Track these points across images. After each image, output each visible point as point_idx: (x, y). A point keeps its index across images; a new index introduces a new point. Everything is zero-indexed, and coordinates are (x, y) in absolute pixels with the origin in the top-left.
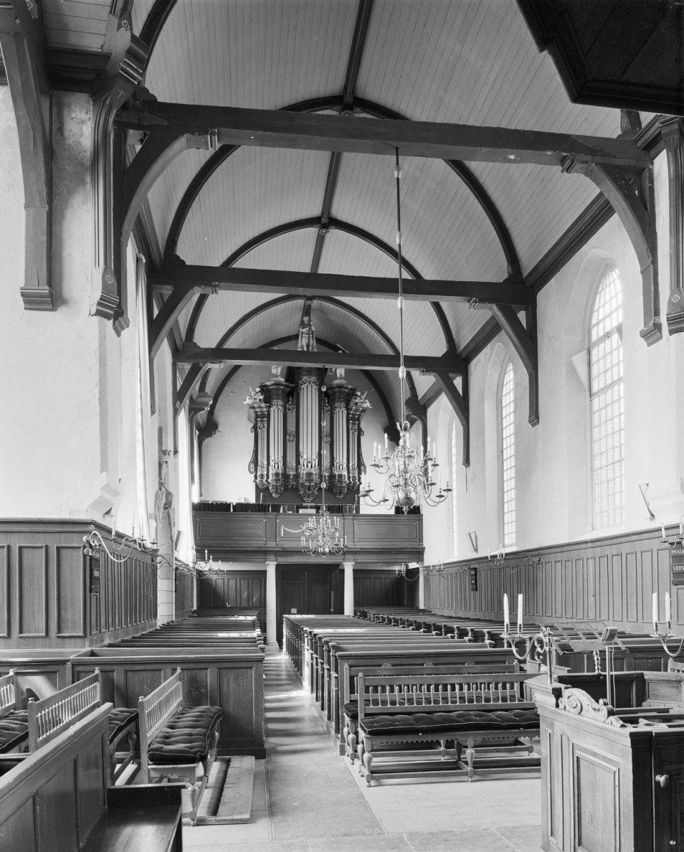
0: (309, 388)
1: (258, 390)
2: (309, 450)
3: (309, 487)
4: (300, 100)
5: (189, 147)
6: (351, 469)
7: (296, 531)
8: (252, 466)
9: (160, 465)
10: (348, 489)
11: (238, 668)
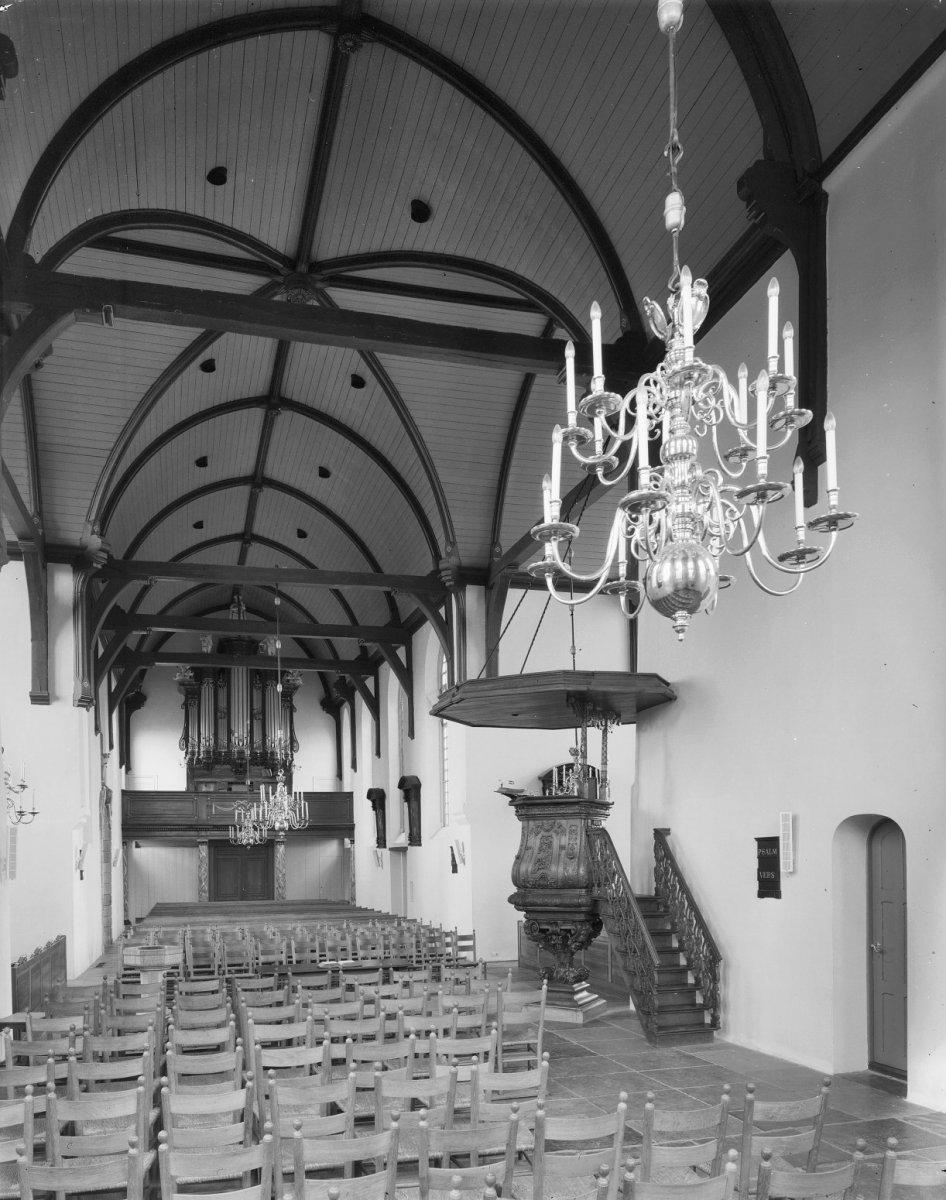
9: (102, 767)
11: (98, 487)
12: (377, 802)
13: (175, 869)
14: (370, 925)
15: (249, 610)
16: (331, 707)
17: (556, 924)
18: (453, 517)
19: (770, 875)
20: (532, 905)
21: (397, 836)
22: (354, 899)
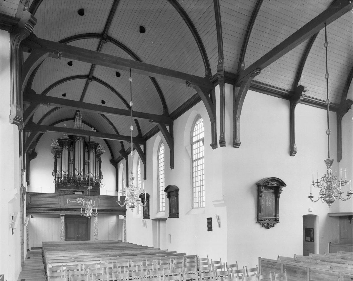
0: (80, 142)
1: (57, 141)
2: (79, 169)
3: (79, 183)
4: (85, 33)
5: (49, 57)
6: (97, 176)
7: (74, 202)
8: (54, 173)
10: (95, 184)
13: (49, 229)
15: (84, 122)
16: (115, 163)
18: (224, 44)
19: (210, 226)
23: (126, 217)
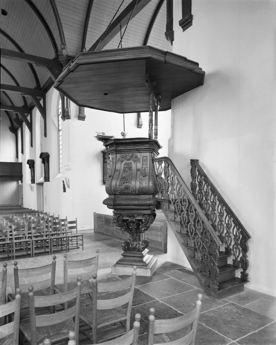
12: (31, 165)
14: (24, 216)
16: (14, 130)
17: (133, 216)
20: (119, 205)
21: (39, 178)
22: (22, 204)
23: (22, 183)
